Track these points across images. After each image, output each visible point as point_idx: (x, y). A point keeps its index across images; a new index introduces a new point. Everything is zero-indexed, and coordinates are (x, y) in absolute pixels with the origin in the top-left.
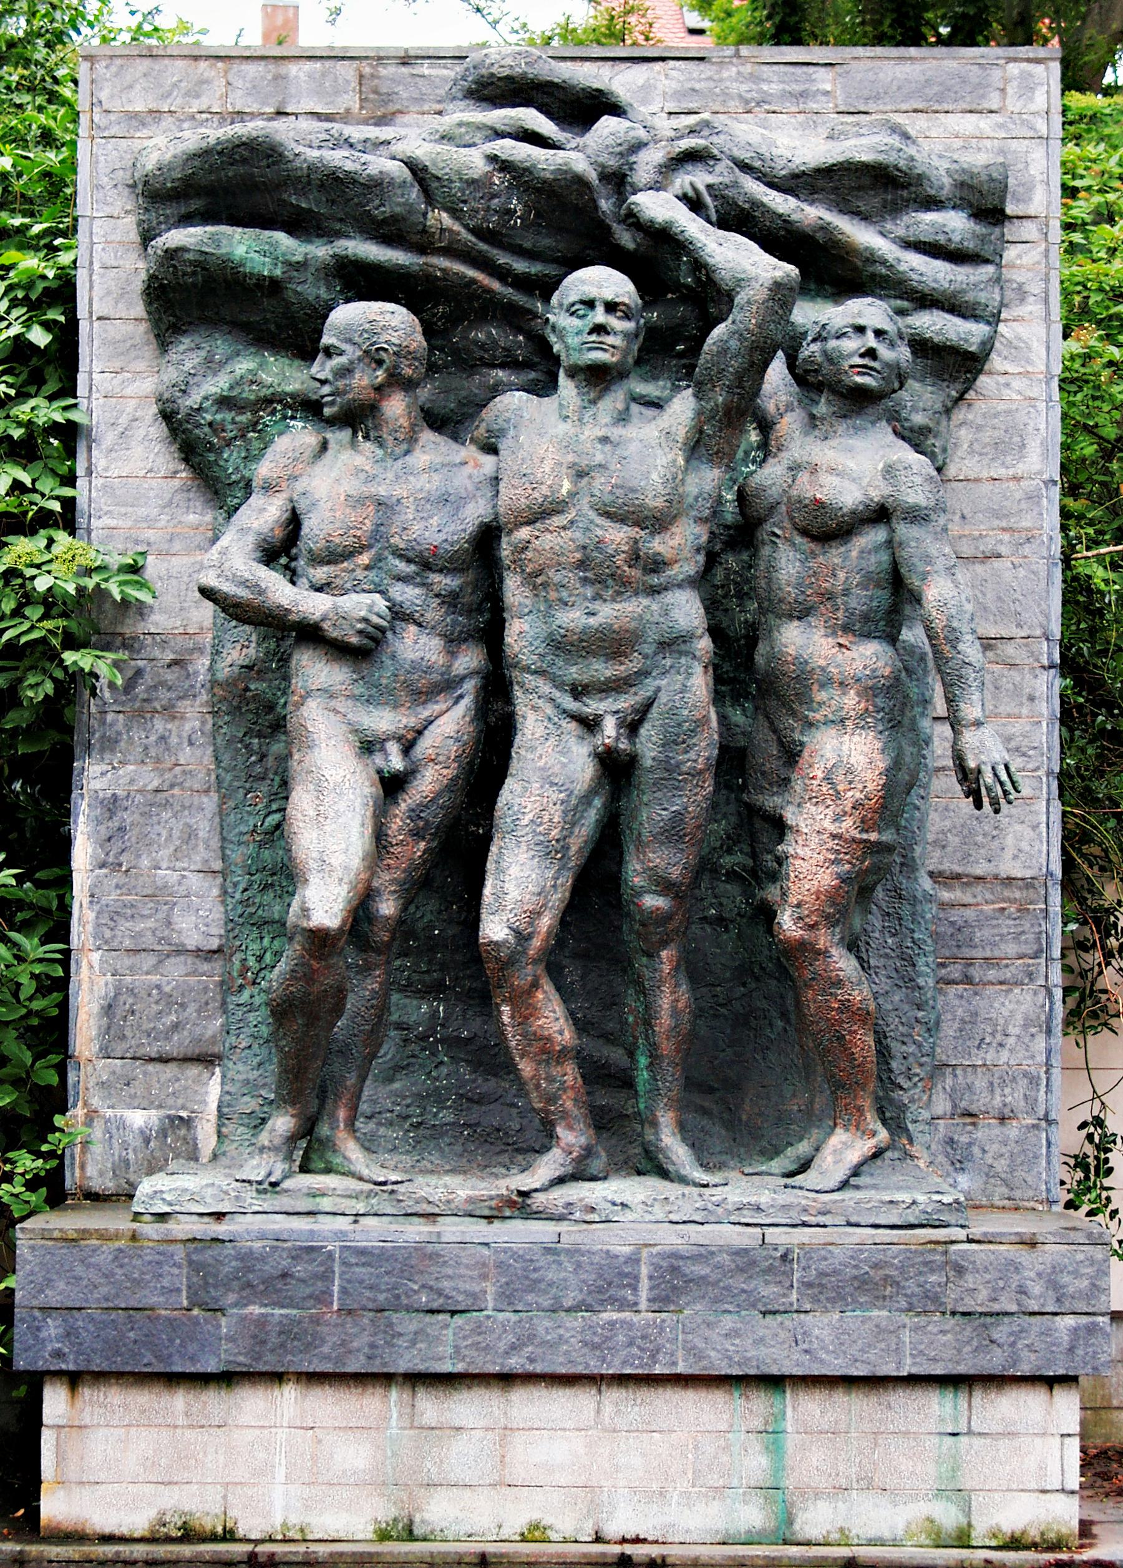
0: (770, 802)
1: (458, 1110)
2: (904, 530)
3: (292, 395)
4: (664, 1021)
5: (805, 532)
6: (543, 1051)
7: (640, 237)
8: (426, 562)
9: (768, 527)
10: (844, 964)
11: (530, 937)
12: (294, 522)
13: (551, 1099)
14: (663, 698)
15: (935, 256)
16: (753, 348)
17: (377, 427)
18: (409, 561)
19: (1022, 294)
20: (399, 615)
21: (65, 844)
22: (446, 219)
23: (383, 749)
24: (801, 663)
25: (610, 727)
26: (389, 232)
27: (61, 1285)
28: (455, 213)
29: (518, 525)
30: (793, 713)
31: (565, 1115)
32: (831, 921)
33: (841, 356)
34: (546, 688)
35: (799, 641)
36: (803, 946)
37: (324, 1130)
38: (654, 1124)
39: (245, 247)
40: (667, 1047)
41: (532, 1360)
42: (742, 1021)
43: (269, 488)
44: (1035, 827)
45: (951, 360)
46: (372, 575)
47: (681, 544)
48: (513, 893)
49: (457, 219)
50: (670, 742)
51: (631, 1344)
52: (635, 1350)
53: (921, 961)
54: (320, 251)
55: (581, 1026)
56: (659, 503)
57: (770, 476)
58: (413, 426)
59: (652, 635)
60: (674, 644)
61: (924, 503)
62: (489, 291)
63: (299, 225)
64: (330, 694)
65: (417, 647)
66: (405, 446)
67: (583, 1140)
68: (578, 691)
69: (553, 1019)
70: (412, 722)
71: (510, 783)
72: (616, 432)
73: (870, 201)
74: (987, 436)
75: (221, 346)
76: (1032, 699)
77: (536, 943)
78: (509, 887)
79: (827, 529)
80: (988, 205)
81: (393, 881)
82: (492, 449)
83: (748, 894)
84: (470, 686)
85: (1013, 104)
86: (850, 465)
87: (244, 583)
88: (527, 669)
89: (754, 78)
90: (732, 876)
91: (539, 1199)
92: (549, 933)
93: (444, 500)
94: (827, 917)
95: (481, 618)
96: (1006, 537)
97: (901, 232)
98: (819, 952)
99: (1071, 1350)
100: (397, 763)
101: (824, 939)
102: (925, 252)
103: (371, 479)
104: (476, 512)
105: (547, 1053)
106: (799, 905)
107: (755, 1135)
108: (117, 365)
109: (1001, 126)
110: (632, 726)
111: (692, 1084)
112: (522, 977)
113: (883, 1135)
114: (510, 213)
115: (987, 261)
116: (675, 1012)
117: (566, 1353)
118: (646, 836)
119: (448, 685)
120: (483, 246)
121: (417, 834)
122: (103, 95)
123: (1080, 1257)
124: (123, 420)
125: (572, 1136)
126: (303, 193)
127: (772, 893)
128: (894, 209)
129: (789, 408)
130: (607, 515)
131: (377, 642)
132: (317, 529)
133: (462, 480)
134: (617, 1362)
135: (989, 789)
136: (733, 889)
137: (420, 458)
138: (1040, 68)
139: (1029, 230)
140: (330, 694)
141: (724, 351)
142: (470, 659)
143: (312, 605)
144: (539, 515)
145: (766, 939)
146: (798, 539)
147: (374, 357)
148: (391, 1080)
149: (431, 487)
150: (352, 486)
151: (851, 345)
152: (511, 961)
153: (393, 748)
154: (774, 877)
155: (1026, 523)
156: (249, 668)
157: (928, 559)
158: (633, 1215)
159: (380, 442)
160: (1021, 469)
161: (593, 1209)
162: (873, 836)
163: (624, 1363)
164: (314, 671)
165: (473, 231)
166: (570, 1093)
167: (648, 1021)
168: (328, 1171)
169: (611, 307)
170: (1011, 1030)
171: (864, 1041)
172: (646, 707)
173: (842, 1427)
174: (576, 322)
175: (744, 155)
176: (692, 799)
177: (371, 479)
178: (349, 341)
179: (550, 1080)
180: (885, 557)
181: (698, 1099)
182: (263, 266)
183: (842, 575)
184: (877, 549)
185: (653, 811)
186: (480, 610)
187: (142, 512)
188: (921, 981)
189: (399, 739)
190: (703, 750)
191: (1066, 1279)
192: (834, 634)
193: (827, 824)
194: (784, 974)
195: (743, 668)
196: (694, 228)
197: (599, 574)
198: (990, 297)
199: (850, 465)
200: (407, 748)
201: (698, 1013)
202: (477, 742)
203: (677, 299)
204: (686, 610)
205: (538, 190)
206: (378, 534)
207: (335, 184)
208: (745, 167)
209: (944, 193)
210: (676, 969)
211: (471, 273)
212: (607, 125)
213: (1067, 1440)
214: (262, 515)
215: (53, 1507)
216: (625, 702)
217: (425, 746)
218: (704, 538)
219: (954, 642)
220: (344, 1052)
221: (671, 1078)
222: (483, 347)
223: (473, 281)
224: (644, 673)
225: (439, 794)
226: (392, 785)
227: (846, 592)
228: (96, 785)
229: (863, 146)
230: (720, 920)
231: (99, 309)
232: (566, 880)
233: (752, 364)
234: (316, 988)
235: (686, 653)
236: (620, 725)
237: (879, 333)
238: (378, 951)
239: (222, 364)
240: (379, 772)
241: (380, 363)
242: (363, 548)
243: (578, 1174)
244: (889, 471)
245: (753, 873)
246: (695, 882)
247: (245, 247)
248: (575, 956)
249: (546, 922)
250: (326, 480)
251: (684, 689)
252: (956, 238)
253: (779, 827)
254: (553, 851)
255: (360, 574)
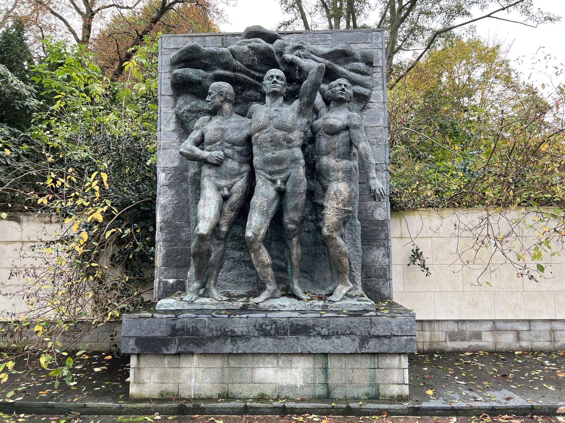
0: (320, 202)
1: (246, 278)
2: (353, 131)
3: (206, 110)
4: (294, 257)
5: (327, 133)
6: (263, 265)
7: (286, 65)
8: (233, 144)
9: (318, 134)
10: (340, 241)
11: (258, 235)
12: (203, 136)
13: (265, 277)
14: (292, 174)
15: (357, 73)
16: (313, 85)
17: (222, 112)
18: (229, 143)
19: (377, 84)
20: (226, 156)
21: (155, 215)
22: (239, 63)
23: (223, 189)
24: (327, 166)
25: (279, 182)
26: (226, 66)
27: (134, 330)
28: (241, 61)
29: (255, 133)
30: (325, 179)
31: (269, 281)
32: (337, 230)
33: (336, 91)
34: (263, 173)
35: (326, 161)
36: (329, 237)
37: (207, 286)
38: (292, 283)
39: (191, 73)
40: (295, 263)
41: (259, 350)
42: (315, 256)
43: (197, 128)
44: (384, 209)
45: (362, 97)
46: (220, 147)
47: (297, 136)
48: (254, 224)
49: (242, 63)
50: (294, 185)
51: (286, 345)
52: (287, 347)
53: (357, 241)
54: (210, 74)
55: (272, 257)
56: (290, 125)
57: (319, 122)
58: (231, 112)
59: (289, 159)
60: (295, 161)
61: (358, 124)
62: (250, 81)
63: (206, 68)
64: (209, 176)
65: (232, 165)
66: (228, 116)
67: (274, 288)
68: (271, 173)
69: (265, 256)
70: (230, 183)
71: (254, 197)
72: (279, 109)
73: (341, 60)
74: (370, 117)
75: (188, 98)
76: (382, 178)
77: (260, 237)
78: (253, 222)
79: (333, 132)
80: (370, 63)
81: (225, 222)
82: (250, 117)
83: (315, 225)
84: (245, 174)
85: (374, 41)
86: (337, 117)
87: (189, 150)
88: (258, 169)
89: (313, 37)
90: (311, 221)
91: (262, 305)
92: (263, 234)
93: (238, 129)
94: (336, 229)
95: (248, 157)
96: (375, 140)
97: (349, 67)
98: (333, 238)
99: (406, 346)
100: (226, 192)
101: (335, 235)
102: (355, 72)
103: (220, 124)
104: (246, 132)
105: (264, 266)
106: (328, 226)
107: (318, 283)
108: (167, 106)
109: (372, 46)
110: (285, 182)
111: (302, 271)
112: (256, 247)
113: (351, 285)
114: (254, 60)
115: (369, 75)
116: (297, 254)
117: (269, 347)
118: (289, 210)
119: (240, 174)
120: (248, 69)
121: (232, 211)
122: (164, 45)
123: (407, 320)
124: (168, 118)
125: (271, 287)
126: (205, 59)
127: (321, 224)
128: (347, 62)
129: (323, 107)
130: (277, 128)
131: (221, 163)
132: (207, 136)
133: (243, 125)
134: (282, 350)
135: (378, 195)
136: (312, 224)
137: (233, 119)
138: (380, 33)
139: (379, 70)
140: (209, 176)
141: (306, 87)
142: (245, 168)
143: (205, 154)
144: (260, 130)
145: (320, 236)
146: (326, 135)
147: (220, 94)
148: (230, 271)
149: (233, 126)
150: (215, 126)
151: (338, 88)
152: (253, 242)
153: (225, 189)
154: (321, 220)
155: (380, 137)
156: (196, 173)
157: (359, 138)
158: (285, 308)
159: (223, 115)
160: (378, 124)
161: (275, 307)
162: (347, 208)
163: (284, 350)
164: (206, 171)
165: (245, 66)
166: (270, 276)
167: (290, 256)
168: (208, 297)
169: (278, 77)
170: (380, 257)
171: (346, 261)
172: (288, 177)
173: (344, 367)
174: (269, 81)
175: (312, 50)
176: (301, 199)
177: (220, 124)
178: (215, 90)
179: (265, 272)
180: (348, 139)
181: (304, 275)
182: (197, 78)
183: (337, 143)
184: (346, 137)
185: (290, 203)
186: (248, 156)
187: (172, 139)
188: (358, 245)
189: (227, 187)
190: (303, 187)
191: (404, 326)
192: (335, 158)
193: (335, 205)
194: (324, 244)
195: (315, 172)
196: (298, 59)
197: (275, 143)
198: (371, 83)
199: (337, 117)
200: (229, 189)
201: (303, 254)
202: (247, 188)
203: (294, 74)
204: (298, 153)
205: (260, 53)
206: (222, 137)
207: (212, 55)
208: (312, 52)
209: (359, 58)
210: (297, 243)
211: (246, 77)
212: (278, 41)
213: (405, 370)
214: (195, 135)
215: (133, 390)
216: (283, 176)
217: (234, 188)
218: (302, 136)
219: (367, 157)
220: (213, 266)
221: (297, 271)
222: (249, 96)
223: (246, 79)
224: (287, 168)
225: (237, 200)
226: (225, 199)
227: (338, 148)
228: (162, 202)
229: (340, 47)
230: (309, 231)
231: (163, 93)
232: (268, 221)
233: (313, 89)
234: (201, 250)
235: (298, 163)
236: (281, 182)
237: (345, 85)
238: (222, 240)
239: (189, 102)
240: (222, 195)
241: (222, 95)
242: (218, 141)
243: (273, 297)
244: (349, 117)
245: (316, 220)
246: (302, 221)
247: (191, 73)
248: (274, 240)
249: (263, 232)
250: (210, 127)
251: (298, 172)
252: (362, 68)
253: (322, 207)
254: (264, 213)
255: (217, 147)
